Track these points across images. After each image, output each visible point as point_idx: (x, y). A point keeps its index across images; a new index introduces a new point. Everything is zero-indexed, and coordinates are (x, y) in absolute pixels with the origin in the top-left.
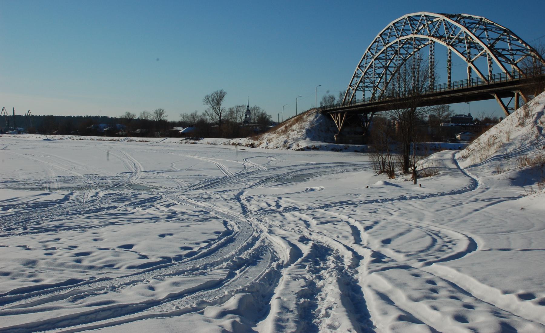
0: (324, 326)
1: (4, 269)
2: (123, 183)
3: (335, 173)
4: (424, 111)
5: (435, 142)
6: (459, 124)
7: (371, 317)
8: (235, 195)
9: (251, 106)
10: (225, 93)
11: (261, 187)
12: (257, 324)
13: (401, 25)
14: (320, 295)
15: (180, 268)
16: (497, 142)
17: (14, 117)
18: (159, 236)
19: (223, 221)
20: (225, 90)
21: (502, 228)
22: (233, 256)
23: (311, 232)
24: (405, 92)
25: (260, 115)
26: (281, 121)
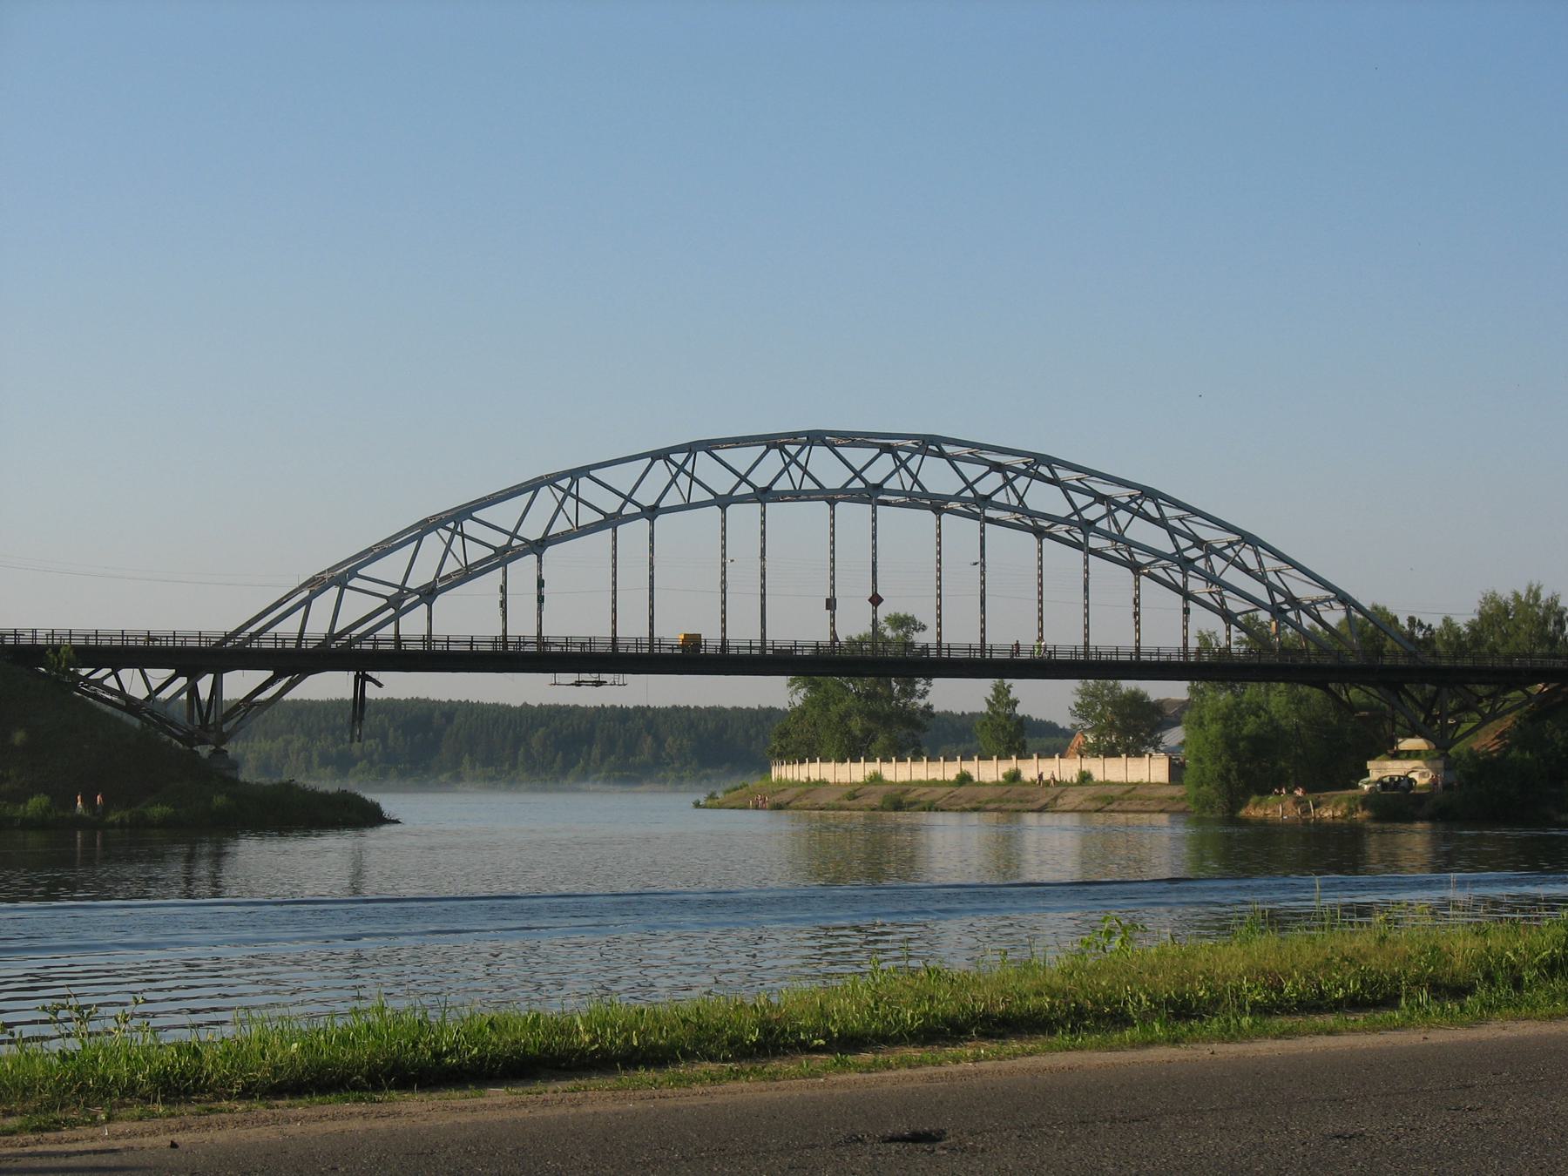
0: (887, 630)
1: (164, 998)
2: (1308, 932)
3: (631, 912)
4: (284, 1042)
5: (75, 841)
6: (479, 1049)
7: (700, 635)
8: (809, 779)
9: (887, 615)
10: (1019, 702)
11: (393, 988)
12: (1069, 728)
13: (1314, 890)
14: (900, 730)
15: (822, 1060)
16: (207, 697)
17: (348, 671)
18: (400, 823)
19: (1185, 782)
20: (1019, 699)
21: (576, 837)
22: (922, 1075)
23: (136, 995)
24: (76, 1101)
25: (288, 1098)
26: (960, 634)
